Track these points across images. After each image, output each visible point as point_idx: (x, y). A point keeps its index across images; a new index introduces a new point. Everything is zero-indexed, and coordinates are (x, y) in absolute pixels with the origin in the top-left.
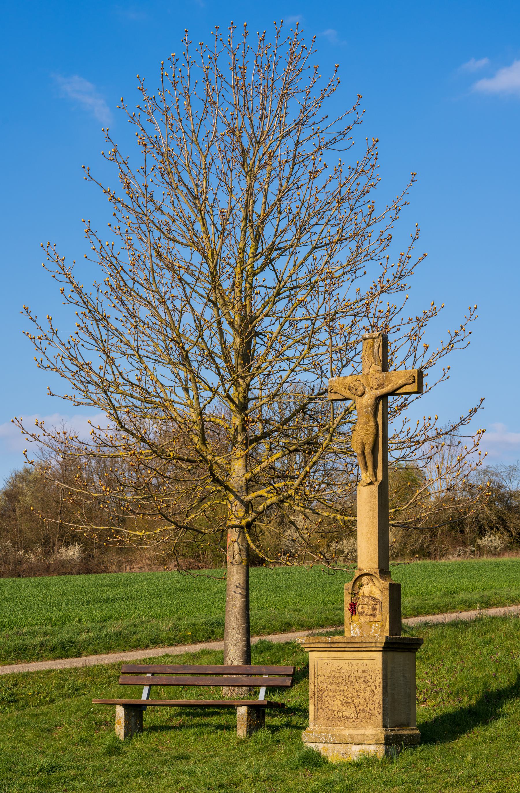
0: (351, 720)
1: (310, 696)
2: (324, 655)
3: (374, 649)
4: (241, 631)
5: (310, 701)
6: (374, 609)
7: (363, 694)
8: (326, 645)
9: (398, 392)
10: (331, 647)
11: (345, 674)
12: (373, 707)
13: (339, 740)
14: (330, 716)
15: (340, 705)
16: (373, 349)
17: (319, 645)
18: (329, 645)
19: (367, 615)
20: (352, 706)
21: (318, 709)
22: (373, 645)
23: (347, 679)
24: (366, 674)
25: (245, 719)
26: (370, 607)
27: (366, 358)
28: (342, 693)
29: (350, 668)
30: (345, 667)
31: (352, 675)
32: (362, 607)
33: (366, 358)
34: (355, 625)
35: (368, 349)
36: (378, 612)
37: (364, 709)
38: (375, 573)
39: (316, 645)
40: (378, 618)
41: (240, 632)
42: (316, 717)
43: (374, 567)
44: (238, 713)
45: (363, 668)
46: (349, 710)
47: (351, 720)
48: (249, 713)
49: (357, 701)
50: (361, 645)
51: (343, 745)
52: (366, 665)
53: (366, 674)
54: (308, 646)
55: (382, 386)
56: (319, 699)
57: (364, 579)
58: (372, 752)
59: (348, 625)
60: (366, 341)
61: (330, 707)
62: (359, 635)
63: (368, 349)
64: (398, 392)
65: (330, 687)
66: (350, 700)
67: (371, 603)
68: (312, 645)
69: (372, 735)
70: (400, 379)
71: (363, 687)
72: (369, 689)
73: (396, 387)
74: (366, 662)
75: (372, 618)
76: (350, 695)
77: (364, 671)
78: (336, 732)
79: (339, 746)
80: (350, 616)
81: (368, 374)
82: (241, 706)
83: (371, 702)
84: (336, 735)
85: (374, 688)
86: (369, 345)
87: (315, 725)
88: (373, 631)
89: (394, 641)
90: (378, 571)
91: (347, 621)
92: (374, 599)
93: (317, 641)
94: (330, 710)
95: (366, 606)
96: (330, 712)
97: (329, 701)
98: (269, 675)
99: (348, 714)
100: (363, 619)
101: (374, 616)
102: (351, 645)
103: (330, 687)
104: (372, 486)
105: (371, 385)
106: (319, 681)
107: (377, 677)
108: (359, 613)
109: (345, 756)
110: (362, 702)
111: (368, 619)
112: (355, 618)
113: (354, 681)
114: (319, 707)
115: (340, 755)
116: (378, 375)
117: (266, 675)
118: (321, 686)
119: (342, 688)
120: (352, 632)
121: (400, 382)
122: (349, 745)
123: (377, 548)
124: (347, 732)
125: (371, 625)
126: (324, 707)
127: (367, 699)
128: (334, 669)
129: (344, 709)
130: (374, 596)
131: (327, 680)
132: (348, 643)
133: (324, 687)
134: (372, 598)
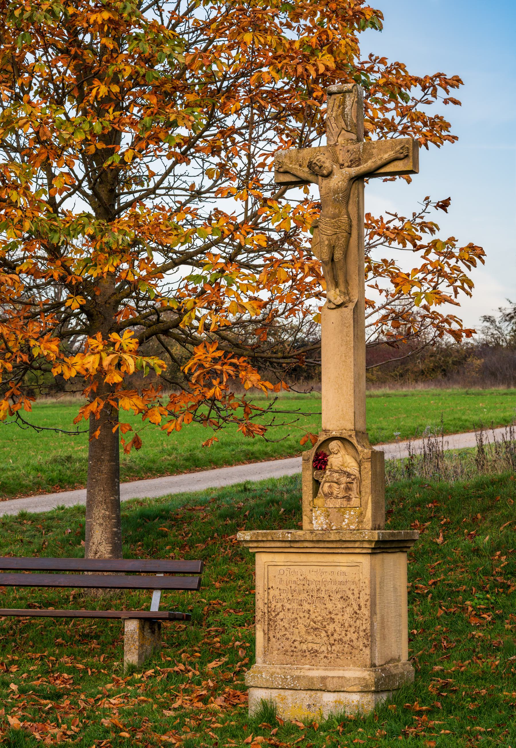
0: (322, 656)
1: (258, 618)
2: (280, 559)
3: (358, 551)
4: (110, 505)
5: (258, 626)
6: (348, 489)
7: (339, 616)
8: (283, 545)
9: (382, 171)
10: (292, 546)
11: (312, 586)
12: (355, 636)
13: (304, 684)
14: (288, 648)
15: (303, 633)
16: (344, 108)
17: (273, 545)
18: (288, 545)
19: (337, 497)
20: (323, 634)
21: (269, 638)
22: (357, 545)
23: (315, 594)
24: (344, 587)
25: (136, 636)
26: (342, 486)
27: (333, 121)
28: (307, 616)
29: (320, 579)
30: (311, 577)
31: (323, 588)
32: (330, 487)
33: (333, 121)
34: (318, 512)
35: (335, 108)
36: (353, 494)
37: (341, 640)
38: (350, 436)
39: (268, 545)
40: (355, 501)
41: (107, 507)
42: (266, 651)
43: (348, 428)
44: (126, 630)
45: (341, 578)
46: (317, 640)
47: (322, 656)
48: (142, 629)
49: (331, 628)
50: (338, 545)
51: (309, 692)
52: (344, 574)
53: (344, 587)
54: (255, 545)
55: (356, 162)
56: (271, 623)
57: (334, 445)
58: (355, 703)
59: (309, 513)
60: (333, 97)
61: (288, 636)
62: (325, 526)
63: (335, 108)
64: (382, 171)
65: (288, 606)
66: (319, 625)
67: (344, 479)
68: (261, 545)
69: (355, 678)
70: (386, 152)
71: (339, 606)
72: (349, 610)
73: (379, 163)
74: (344, 569)
75: (345, 503)
76: (320, 618)
77: (341, 583)
78: (297, 673)
79: (303, 694)
80: (311, 499)
81: (335, 145)
82: (131, 618)
83: (352, 629)
84: (298, 677)
85: (356, 608)
86: (337, 103)
87: (264, 662)
88: (346, 520)
89: (387, 538)
90: (353, 433)
91: (306, 507)
92: (349, 475)
93: (270, 538)
94: (287, 639)
95: (335, 485)
96: (288, 643)
97: (287, 626)
98: (165, 572)
99: (316, 647)
100: (331, 503)
101: (349, 499)
102: (322, 545)
103: (288, 606)
104: (343, 309)
105: (341, 162)
106: (271, 597)
107: (363, 593)
108: (325, 495)
109: (313, 708)
110: (337, 629)
111: (338, 503)
112: (318, 502)
113: (326, 597)
114: (271, 635)
115: (305, 707)
116: (351, 147)
117: (160, 572)
118: (274, 603)
119: (306, 606)
120: (314, 522)
121: (386, 157)
122: (319, 693)
123: (352, 399)
124: (317, 673)
125: (344, 513)
126: (278, 636)
127: (346, 625)
128: (294, 579)
129: (310, 638)
130: (348, 470)
131: (284, 595)
132: (318, 541)
133: (279, 605)
134: (345, 472)
